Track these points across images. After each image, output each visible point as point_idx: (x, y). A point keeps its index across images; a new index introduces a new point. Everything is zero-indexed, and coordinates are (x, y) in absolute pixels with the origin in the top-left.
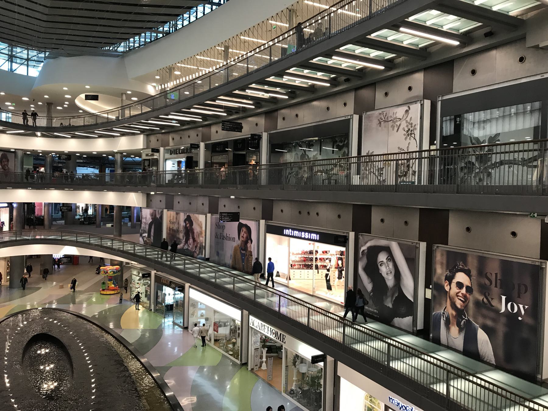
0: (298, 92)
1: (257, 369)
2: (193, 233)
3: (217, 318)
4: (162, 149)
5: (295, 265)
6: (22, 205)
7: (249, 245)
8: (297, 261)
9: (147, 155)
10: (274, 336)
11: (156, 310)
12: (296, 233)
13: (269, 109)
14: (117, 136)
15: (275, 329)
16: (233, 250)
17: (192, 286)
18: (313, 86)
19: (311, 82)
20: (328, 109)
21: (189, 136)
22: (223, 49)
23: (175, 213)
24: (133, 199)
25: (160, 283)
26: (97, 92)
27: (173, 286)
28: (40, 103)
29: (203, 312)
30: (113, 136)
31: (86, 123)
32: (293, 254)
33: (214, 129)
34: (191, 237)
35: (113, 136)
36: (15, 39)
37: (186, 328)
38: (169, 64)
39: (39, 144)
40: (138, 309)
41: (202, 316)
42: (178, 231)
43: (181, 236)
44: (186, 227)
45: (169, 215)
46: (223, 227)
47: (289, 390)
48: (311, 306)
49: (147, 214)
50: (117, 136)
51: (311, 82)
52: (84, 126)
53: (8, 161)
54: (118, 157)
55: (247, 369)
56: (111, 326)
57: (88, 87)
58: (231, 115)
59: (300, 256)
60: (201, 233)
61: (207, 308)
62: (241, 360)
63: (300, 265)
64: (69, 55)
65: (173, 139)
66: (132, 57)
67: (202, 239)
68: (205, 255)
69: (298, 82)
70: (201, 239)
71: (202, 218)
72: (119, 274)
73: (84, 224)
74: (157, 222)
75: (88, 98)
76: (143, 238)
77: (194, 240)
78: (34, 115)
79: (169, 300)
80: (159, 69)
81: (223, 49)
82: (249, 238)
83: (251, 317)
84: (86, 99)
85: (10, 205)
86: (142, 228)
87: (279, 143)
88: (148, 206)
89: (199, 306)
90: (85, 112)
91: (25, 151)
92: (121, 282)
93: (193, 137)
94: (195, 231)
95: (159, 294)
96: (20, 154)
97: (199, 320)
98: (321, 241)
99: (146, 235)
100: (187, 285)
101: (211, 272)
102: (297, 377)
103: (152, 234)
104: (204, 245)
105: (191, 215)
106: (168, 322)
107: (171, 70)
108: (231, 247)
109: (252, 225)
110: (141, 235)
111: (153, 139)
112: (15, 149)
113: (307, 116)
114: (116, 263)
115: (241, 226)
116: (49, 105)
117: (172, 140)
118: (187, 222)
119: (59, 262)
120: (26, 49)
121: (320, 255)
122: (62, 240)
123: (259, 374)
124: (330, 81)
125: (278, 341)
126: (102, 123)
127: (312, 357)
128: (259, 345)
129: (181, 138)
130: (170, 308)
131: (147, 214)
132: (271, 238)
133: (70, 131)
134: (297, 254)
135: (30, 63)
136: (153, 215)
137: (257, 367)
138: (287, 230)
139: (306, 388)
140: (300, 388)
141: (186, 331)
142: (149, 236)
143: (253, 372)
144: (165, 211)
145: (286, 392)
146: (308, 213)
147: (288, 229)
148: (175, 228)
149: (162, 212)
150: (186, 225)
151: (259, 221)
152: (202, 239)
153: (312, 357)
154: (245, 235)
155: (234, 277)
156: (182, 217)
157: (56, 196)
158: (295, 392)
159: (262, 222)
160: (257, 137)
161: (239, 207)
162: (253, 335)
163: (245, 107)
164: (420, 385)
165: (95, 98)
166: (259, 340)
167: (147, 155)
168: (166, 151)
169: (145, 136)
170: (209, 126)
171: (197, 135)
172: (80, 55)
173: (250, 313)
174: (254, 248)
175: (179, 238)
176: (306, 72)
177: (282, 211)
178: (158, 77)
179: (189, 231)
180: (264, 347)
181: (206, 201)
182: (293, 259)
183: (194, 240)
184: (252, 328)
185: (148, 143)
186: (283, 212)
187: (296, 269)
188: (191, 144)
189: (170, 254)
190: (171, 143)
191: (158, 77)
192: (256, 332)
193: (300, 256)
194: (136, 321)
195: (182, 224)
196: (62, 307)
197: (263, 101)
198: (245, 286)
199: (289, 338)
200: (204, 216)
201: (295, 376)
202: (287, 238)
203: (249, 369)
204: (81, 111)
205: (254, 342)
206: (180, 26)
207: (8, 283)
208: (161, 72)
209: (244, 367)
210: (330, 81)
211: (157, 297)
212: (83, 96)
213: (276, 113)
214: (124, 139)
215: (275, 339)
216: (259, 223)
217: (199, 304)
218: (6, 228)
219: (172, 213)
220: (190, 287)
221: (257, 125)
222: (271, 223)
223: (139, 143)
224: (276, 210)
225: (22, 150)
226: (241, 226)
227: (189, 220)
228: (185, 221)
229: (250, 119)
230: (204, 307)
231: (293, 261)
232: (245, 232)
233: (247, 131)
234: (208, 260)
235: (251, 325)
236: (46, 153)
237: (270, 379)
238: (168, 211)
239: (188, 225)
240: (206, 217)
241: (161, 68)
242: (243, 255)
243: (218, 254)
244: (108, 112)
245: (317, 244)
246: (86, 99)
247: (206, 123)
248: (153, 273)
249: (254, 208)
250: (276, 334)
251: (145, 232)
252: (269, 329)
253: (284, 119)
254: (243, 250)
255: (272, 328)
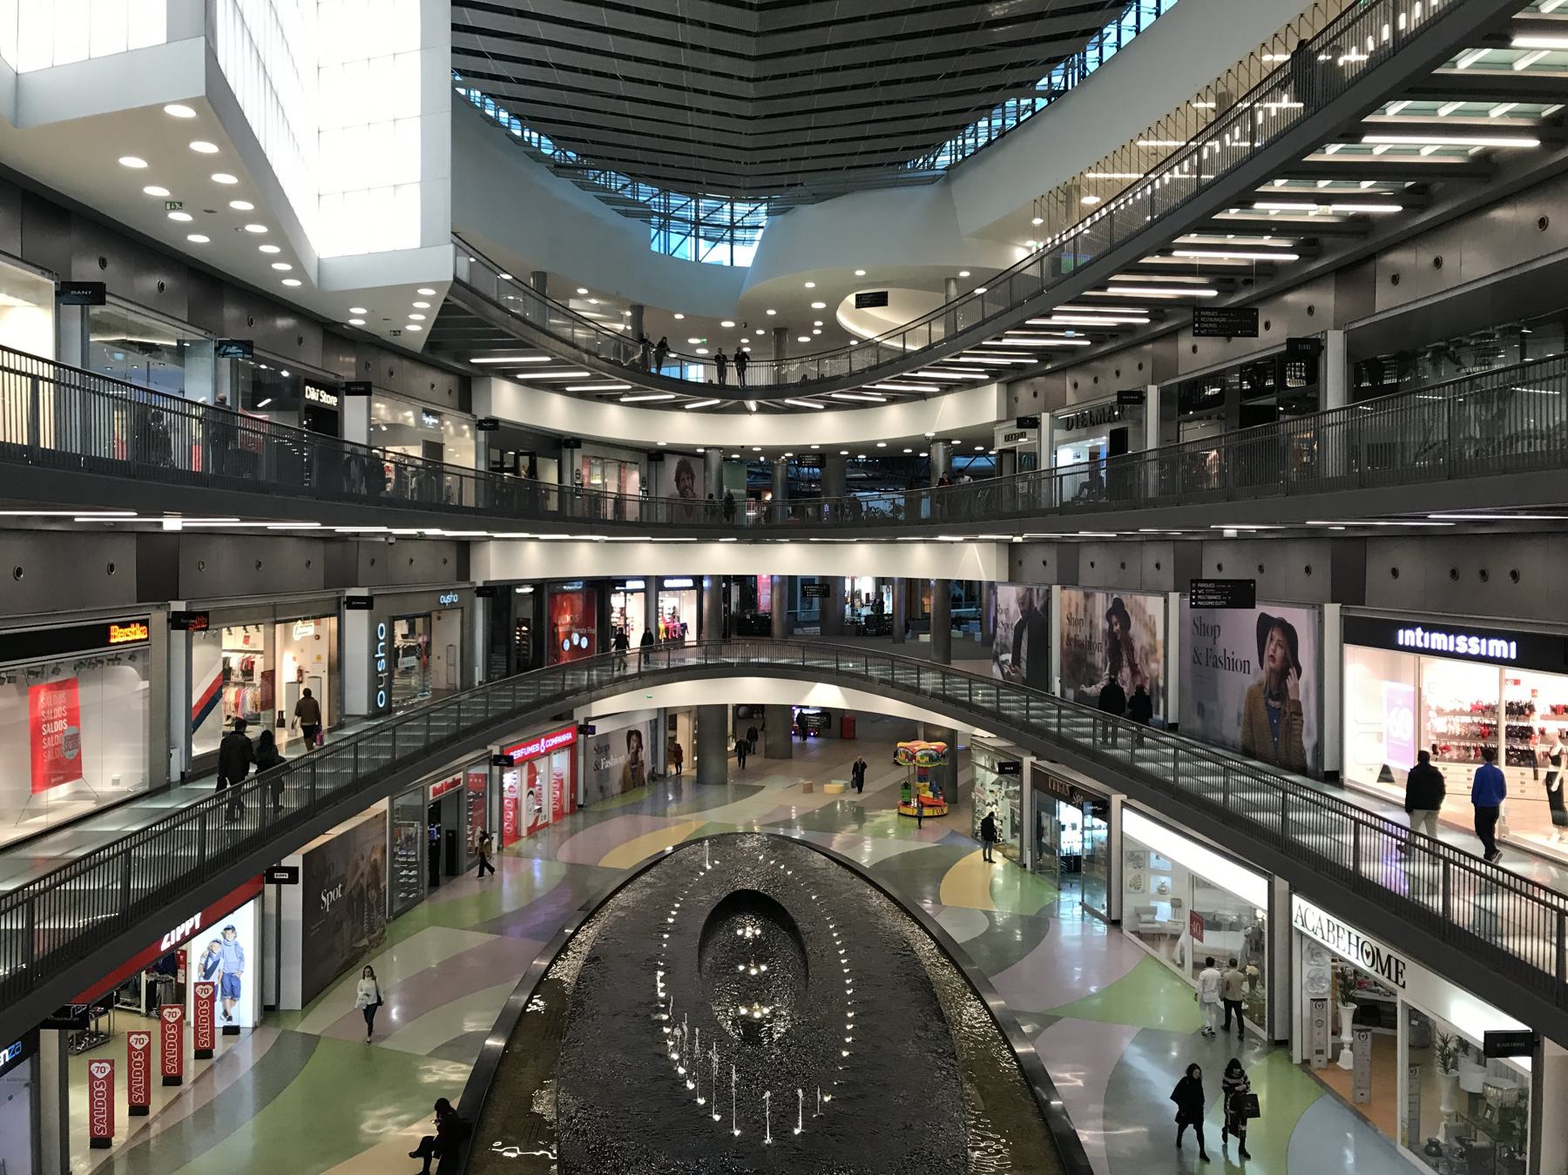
0: (1438, 185)
1: (1322, 1065)
2: (1131, 649)
3: (1204, 903)
4: (1045, 418)
5: (1446, 748)
6: (725, 582)
7: (1290, 683)
8: (1453, 737)
9: (1008, 438)
10: (1369, 962)
11: (1038, 869)
12: (1439, 640)
13: (1343, 255)
14: (934, 395)
15: (1372, 943)
16: (1244, 698)
17: (1133, 802)
18: (1486, 156)
19: (1478, 143)
20: (1543, 223)
21: (1118, 373)
22: (1213, 105)
23: (1081, 593)
24: (974, 560)
25: (1049, 791)
26: (885, 284)
27: (1078, 799)
28: (760, 332)
29: (1166, 880)
30: (923, 396)
31: (856, 368)
32: (1440, 712)
33: (1185, 343)
34: (1125, 663)
35: (923, 396)
36: (694, 176)
37: (1114, 924)
38: (1063, 177)
39: (755, 430)
40: (991, 861)
41: (1162, 891)
42: (1089, 645)
43: (1099, 658)
44: (1110, 634)
45: (1066, 602)
46: (1214, 631)
47: (1424, 1140)
48: (1361, 816)
49: (1009, 599)
50: (934, 395)
51: (1478, 143)
52: (852, 374)
53: (693, 477)
54: (939, 453)
55: (1290, 1059)
56: (928, 905)
57: (860, 273)
58: (1231, 292)
59: (1467, 719)
60: (1154, 650)
61: (1177, 869)
62: (1271, 1031)
63: (1467, 749)
64: (818, 198)
65: (1076, 385)
66: (975, 176)
67: (1156, 667)
68: (1166, 715)
69: (1428, 149)
70: (1153, 666)
71: (1153, 605)
72: (945, 763)
73: (865, 634)
74: (1035, 621)
75: (862, 302)
76: (1001, 665)
77: (1135, 671)
78: (742, 360)
79: (1071, 842)
80: (1037, 196)
81: (1213, 105)
82: (1291, 661)
83: (1297, 901)
84: (858, 306)
85: (698, 580)
86: (998, 639)
87: (1383, 364)
88: (1013, 579)
89: (1154, 863)
90: (862, 341)
91: (726, 451)
92: (946, 780)
93: (1126, 372)
94: (1137, 645)
95: (1045, 823)
96: (715, 458)
97: (1153, 904)
98: (1521, 662)
99: (1008, 657)
100: (1117, 799)
101: (1214, 773)
102: (1451, 1104)
103: (1024, 654)
104: (1161, 683)
105: (1126, 598)
106: (1070, 904)
107: (1070, 192)
108: (1237, 689)
109: (1299, 619)
110: (996, 658)
111: (1023, 392)
112: (706, 448)
113: (1469, 263)
114: (938, 734)
115: (1265, 623)
116: (781, 332)
117: (1075, 391)
118: (1114, 619)
119: (804, 725)
120: (727, 201)
121: (1544, 717)
122: (804, 668)
123: (1327, 1078)
124: (1540, 129)
125: (1383, 978)
126: (891, 362)
127: (1488, 1035)
128: (1325, 989)
129: (1096, 380)
130: (1073, 867)
131: (1009, 599)
132: (1361, 665)
133: (817, 391)
134: (1454, 713)
135: (738, 234)
136: (1025, 603)
137: (1323, 1058)
138: (1409, 633)
139: (1482, 1141)
140: (1459, 1140)
141: (1115, 932)
142: (1016, 660)
143: (1310, 1074)
144: (1056, 589)
145: (1412, 1145)
146: (1483, 573)
147: (1413, 626)
148: (1081, 637)
149: (1048, 592)
150: (1111, 627)
151: (1321, 607)
152: (1156, 667)
153: (1488, 1035)
154: (1279, 652)
155: (1285, 792)
156: (1101, 603)
157: (790, 559)
158: (1445, 1151)
159: (1332, 611)
160: (1308, 347)
161: (1261, 569)
162: (1307, 955)
163: (1271, 263)
164: (1513, 956)
165: (880, 300)
166: (1329, 976)
167: (1008, 438)
168: (1056, 423)
169: (1004, 387)
170: (1172, 334)
171: (1140, 367)
172: (841, 194)
173: (1294, 889)
174: (1307, 691)
175: (1093, 667)
176: (1446, 111)
177: (1395, 572)
178: (1037, 221)
179: (1120, 645)
180: (1348, 999)
181: (1166, 556)
182: (1442, 728)
183: (1135, 671)
184: (1301, 934)
185: (1010, 402)
186: (1399, 574)
187: (1451, 760)
188: (1120, 394)
189: (1100, 726)
190: (1071, 398)
191: (1037, 221)
192: (1317, 949)
193: (1467, 719)
194: (983, 889)
195: (1101, 624)
196: (815, 838)
197: (1322, 232)
198: (1256, 799)
199: (1415, 972)
200: (1162, 599)
201: (1444, 1100)
202: (1411, 657)
203: (1297, 1059)
204: (854, 343)
205: (1308, 982)
206: (1092, 66)
207: (694, 773)
208: (1045, 203)
209: (1280, 1052)
210: (1540, 129)
211: (1039, 831)
212: (851, 299)
213: (1371, 266)
214: (949, 402)
215: (1371, 971)
216: (1321, 615)
217: (1153, 856)
218: (691, 637)
219: (1075, 595)
220: (1124, 804)
221: (1311, 310)
222: (1357, 612)
223: (987, 406)
224: (1376, 571)
225: (719, 448)
226: (1265, 623)
227: (1118, 611)
228: (1108, 616)
229: (1290, 298)
230: (1168, 867)
231: (1440, 736)
232: (1278, 644)
233: (1273, 334)
234: (1173, 728)
235: (1297, 925)
236: (773, 453)
237: (1361, 1099)
238: (1063, 588)
239: (1117, 628)
240: (1166, 602)
241: (1045, 192)
242: (1273, 713)
243: (1201, 710)
244: (901, 333)
245: (1512, 673)
246: (858, 306)
247: (1163, 327)
248: (1028, 761)
249: (1308, 570)
250: (1375, 956)
251: (1005, 650)
252: (1354, 940)
253: (1395, 280)
254: (1274, 699)
255: (1363, 938)
